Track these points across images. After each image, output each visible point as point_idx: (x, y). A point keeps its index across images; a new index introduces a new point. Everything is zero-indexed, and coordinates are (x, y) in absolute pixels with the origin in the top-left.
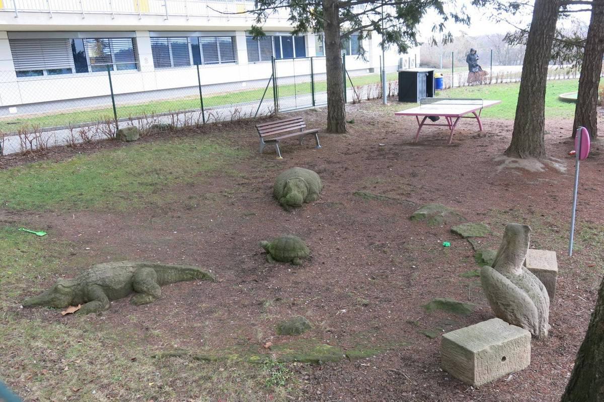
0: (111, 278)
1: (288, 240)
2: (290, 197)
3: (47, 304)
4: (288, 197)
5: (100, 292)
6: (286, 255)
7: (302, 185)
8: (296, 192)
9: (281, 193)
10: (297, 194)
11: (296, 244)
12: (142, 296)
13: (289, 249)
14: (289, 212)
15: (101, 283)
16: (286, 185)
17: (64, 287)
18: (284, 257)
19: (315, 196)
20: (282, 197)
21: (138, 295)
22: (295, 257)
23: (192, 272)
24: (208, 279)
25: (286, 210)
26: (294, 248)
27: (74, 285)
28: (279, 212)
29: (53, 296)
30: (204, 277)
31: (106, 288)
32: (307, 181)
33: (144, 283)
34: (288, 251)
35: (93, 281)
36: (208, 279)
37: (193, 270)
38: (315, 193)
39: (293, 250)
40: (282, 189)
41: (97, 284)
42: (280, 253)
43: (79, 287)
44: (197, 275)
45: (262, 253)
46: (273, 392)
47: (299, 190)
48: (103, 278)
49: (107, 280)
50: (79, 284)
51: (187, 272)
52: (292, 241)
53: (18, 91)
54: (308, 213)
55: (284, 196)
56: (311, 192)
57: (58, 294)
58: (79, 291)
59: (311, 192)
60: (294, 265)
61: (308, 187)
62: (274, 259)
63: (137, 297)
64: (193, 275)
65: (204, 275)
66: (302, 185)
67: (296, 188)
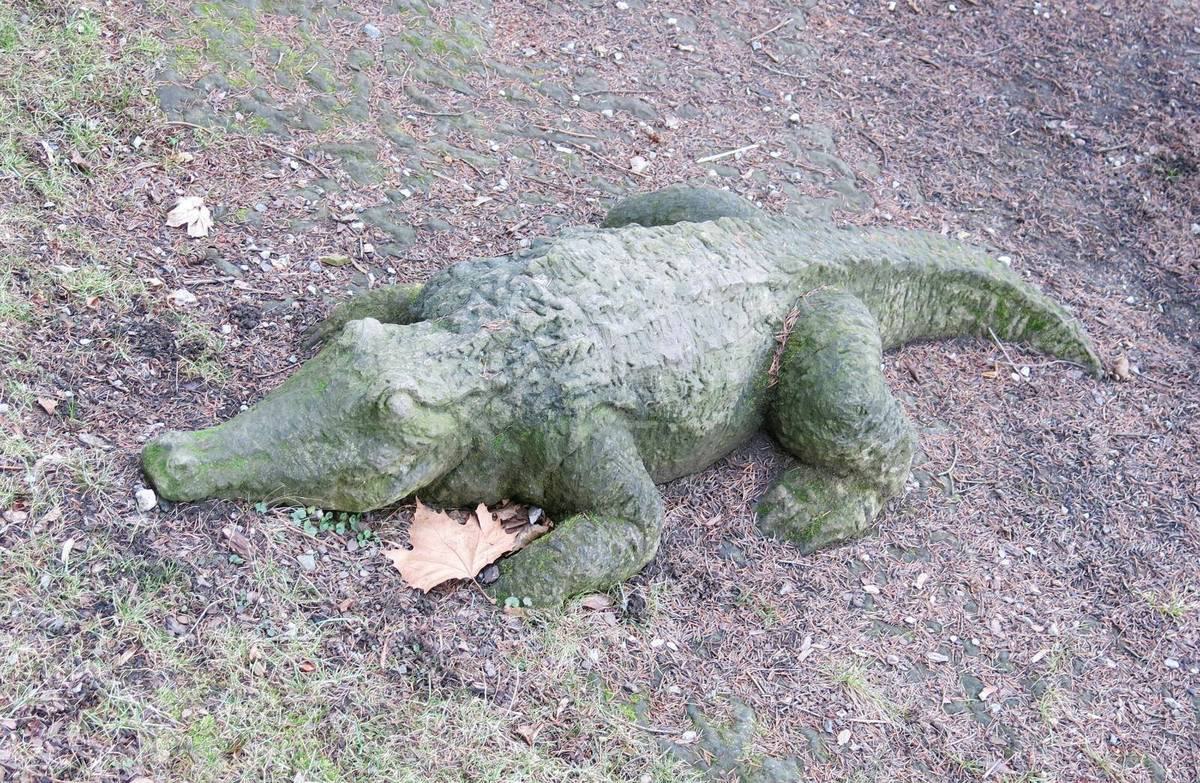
0: (684, 370)
3: (305, 491)
5: (625, 463)
12: (834, 494)
15: (630, 400)
17: (424, 405)
21: (804, 478)
23: (977, 295)
24: (1058, 348)
27: (474, 394)
29: (351, 452)
30: (1037, 333)
31: (645, 425)
33: (871, 427)
35: (595, 387)
36: (1058, 348)
37: (986, 285)
41: (611, 405)
43: (497, 404)
44: (998, 313)
46: (137, 296)
48: (646, 369)
49: (663, 382)
50: (502, 391)
51: (955, 289)
57: (385, 450)
58: (496, 432)
63: (802, 496)
64: (977, 309)
65: (1039, 322)
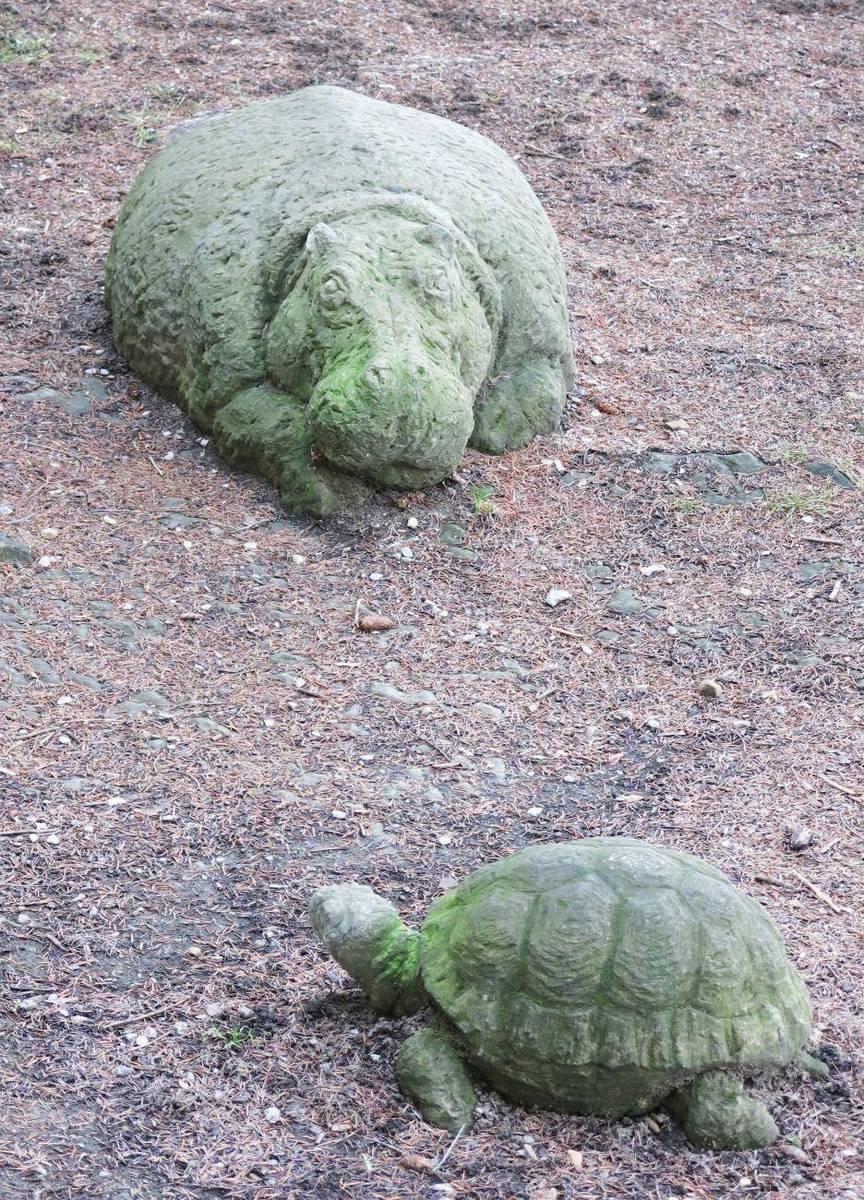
1: (636, 901)
2: (368, 395)
4: (338, 385)
6: (632, 1047)
7: (453, 281)
8: (420, 356)
9: (240, 341)
10: (411, 362)
11: (715, 933)
13: (658, 986)
14: (346, 535)
16: (286, 270)
18: (599, 1065)
19: (552, 384)
20: (247, 383)
22: (712, 1069)
25: (307, 516)
26: (700, 976)
28: (245, 532)
32: (475, 236)
34: (644, 1009)
38: (550, 353)
39: (691, 1001)
40: (240, 304)
42: (567, 1025)
45: (316, 1012)
47: (435, 332)
52: (676, 918)
53: (538, 160)
54: (537, 538)
55: (294, 375)
56: (515, 345)
59: (515, 345)
60: (698, 1144)
61: (496, 290)
62: (481, 1077)
66: (453, 281)
67: (411, 313)
